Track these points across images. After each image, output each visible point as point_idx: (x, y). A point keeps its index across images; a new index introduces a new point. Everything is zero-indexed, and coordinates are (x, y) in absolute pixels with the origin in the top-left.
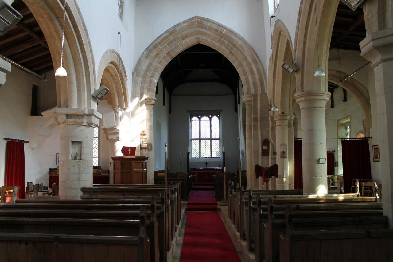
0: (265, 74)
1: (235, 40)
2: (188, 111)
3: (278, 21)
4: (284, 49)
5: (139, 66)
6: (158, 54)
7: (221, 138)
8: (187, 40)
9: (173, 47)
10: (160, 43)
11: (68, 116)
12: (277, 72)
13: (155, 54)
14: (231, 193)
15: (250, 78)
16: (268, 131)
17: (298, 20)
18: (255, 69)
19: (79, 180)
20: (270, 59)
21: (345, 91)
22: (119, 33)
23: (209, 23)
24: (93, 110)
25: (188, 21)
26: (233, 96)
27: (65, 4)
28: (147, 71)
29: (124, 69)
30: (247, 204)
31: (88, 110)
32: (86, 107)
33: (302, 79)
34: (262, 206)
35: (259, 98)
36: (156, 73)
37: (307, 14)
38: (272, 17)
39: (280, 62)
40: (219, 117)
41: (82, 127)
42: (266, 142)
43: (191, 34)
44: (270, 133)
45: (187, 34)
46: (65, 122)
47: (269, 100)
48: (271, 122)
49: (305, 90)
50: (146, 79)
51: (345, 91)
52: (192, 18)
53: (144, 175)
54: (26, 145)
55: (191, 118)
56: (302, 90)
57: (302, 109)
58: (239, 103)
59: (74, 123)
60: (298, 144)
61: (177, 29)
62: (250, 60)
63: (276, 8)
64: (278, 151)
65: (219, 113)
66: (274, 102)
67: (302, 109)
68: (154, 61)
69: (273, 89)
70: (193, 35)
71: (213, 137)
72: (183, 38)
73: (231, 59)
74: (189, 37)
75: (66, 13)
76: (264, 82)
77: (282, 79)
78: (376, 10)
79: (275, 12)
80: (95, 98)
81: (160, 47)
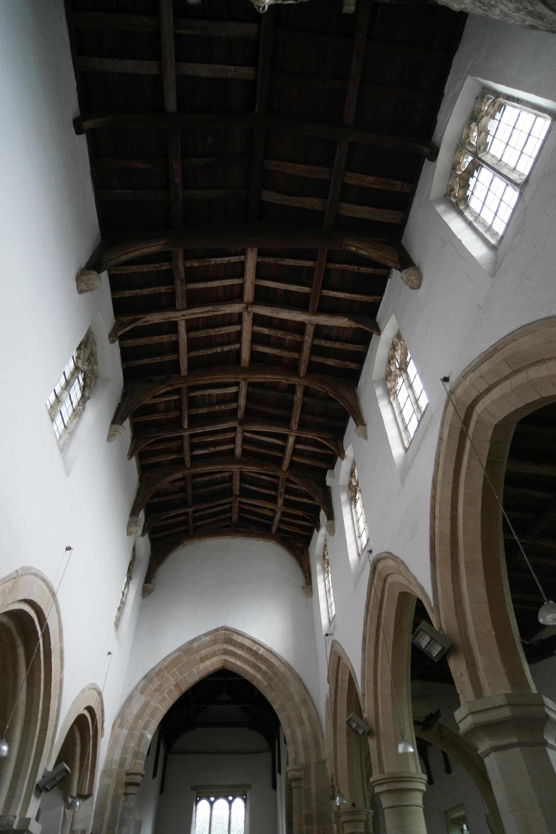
0: (321, 725)
1: (275, 666)
2: (194, 788)
5: (128, 706)
6: (160, 685)
8: (208, 663)
9: (186, 675)
10: (167, 667)
12: (338, 723)
13: (156, 686)
15: (298, 732)
17: (363, 649)
18: (305, 716)
20: (327, 700)
21: (445, 755)
23: (241, 637)
24: (29, 819)
25: (211, 634)
26: (270, 754)
27: (45, 626)
28: (138, 717)
32: (17, 814)
33: (379, 747)
35: (313, 772)
36: (152, 720)
37: (373, 642)
38: (327, 635)
40: (245, 801)
43: (214, 654)
45: (208, 654)
47: (330, 776)
48: (335, 826)
49: (386, 772)
50: (134, 732)
51: (445, 755)
52: (217, 630)
55: (197, 802)
56: (382, 771)
57: (388, 808)
61: (195, 645)
62: (297, 699)
63: (331, 619)
65: (246, 791)
67: (388, 808)
68: (153, 698)
69: (334, 751)
70: (216, 656)
72: (202, 660)
73: (270, 696)
74: (211, 658)
75: (41, 641)
76: (320, 739)
77: (347, 737)
78: (465, 666)
79: (330, 625)
81: (166, 674)
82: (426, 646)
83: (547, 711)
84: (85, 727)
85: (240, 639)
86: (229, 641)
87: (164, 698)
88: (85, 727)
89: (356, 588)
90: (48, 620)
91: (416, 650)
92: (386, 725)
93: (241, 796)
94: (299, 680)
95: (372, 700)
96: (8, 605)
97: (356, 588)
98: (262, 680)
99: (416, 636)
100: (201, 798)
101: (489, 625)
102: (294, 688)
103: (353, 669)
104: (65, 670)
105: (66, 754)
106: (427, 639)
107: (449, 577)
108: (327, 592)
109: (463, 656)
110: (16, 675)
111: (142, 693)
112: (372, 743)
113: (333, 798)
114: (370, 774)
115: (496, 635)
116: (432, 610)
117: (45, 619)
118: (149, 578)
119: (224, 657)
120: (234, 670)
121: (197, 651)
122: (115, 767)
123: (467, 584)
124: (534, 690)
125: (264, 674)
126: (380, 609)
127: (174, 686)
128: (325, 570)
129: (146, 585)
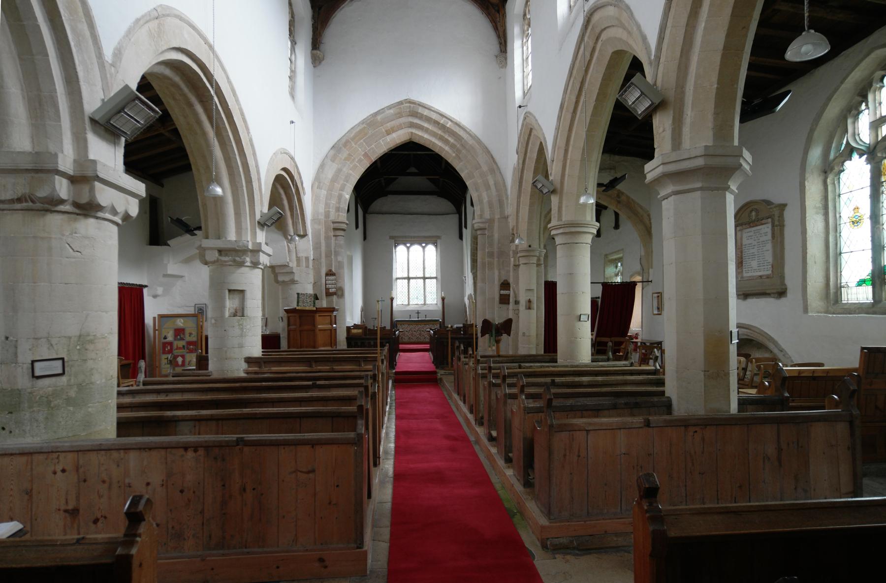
0: (506, 190)
2: (391, 238)
3: (527, 115)
4: (535, 155)
6: (349, 155)
7: (439, 277)
8: (394, 135)
10: (353, 139)
11: (220, 251)
14: (459, 359)
15: (485, 195)
16: (508, 272)
18: (491, 182)
19: (241, 346)
20: (515, 169)
21: (617, 215)
22: (292, 122)
24: (260, 243)
28: (334, 180)
29: (301, 178)
30: (484, 376)
31: (253, 243)
33: (560, 203)
34: (509, 381)
35: (496, 224)
37: (571, 110)
38: (520, 107)
39: (529, 177)
40: (436, 246)
41: (243, 269)
42: (505, 285)
43: (400, 127)
44: (511, 274)
46: (218, 260)
47: (511, 227)
48: (512, 259)
51: (617, 215)
52: (401, 103)
53: (333, 333)
54: (145, 291)
55: (396, 247)
56: (560, 218)
58: (466, 227)
59: (230, 263)
60: (551, 289)
61: (379, 118)
62: (485, 168)
64: (523, 301)
66: (517, 230)
69: (517, 210)
71: (427, 276)
72: (388, 133)
73: (458, 166)
78: (670, 122)
80: (262, 225)
82: (633, 103)
83: (742, 161)
84: (285, 186)
85: (426, 113)
86: (415, 114)
87: (356, 166)
88: (285, 186)
89: (560, 50)
90: (215, 77)
91: (619, 106)
92: (570, 185)
93: (435, 244)
94: (487, 151)
95: (560, 165)
96: (163, 52)
97: (560, 50)
98: (450, 151)
99: (625, 91)
100: (399, 244)
101: (714, 77)
102: (482, 159)
103: (545, 138)
104: (251, 131)
105: (274, 201)
106: (637, 94)
107: (683, 20)
108: (524, 61)
109: (672, 112)
110: (204, 134)
111: (333, 161)
112: (554, 199)
113: (513, 241)
114: (549, 221)
115: (717, 88)
116: (651, 63)
117: (212, 76)
118: (316, 43)
119: (410, 130)
120: (422, 142)
121: (382, 123)
122: (322, 217)
123: (705, 28)
124: (736, 143)
125: (452, 146)
126: (587, 71)
127: (364, 155)
128: (524, 34)
129: (315, 52)
